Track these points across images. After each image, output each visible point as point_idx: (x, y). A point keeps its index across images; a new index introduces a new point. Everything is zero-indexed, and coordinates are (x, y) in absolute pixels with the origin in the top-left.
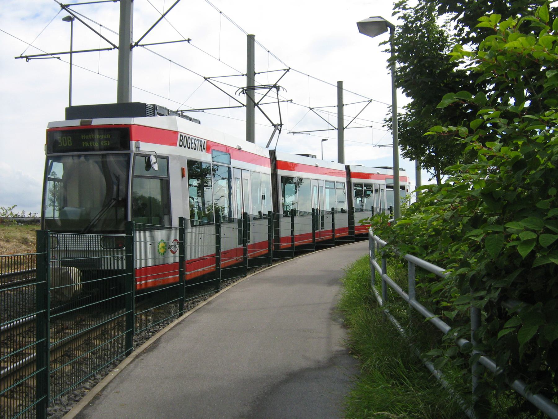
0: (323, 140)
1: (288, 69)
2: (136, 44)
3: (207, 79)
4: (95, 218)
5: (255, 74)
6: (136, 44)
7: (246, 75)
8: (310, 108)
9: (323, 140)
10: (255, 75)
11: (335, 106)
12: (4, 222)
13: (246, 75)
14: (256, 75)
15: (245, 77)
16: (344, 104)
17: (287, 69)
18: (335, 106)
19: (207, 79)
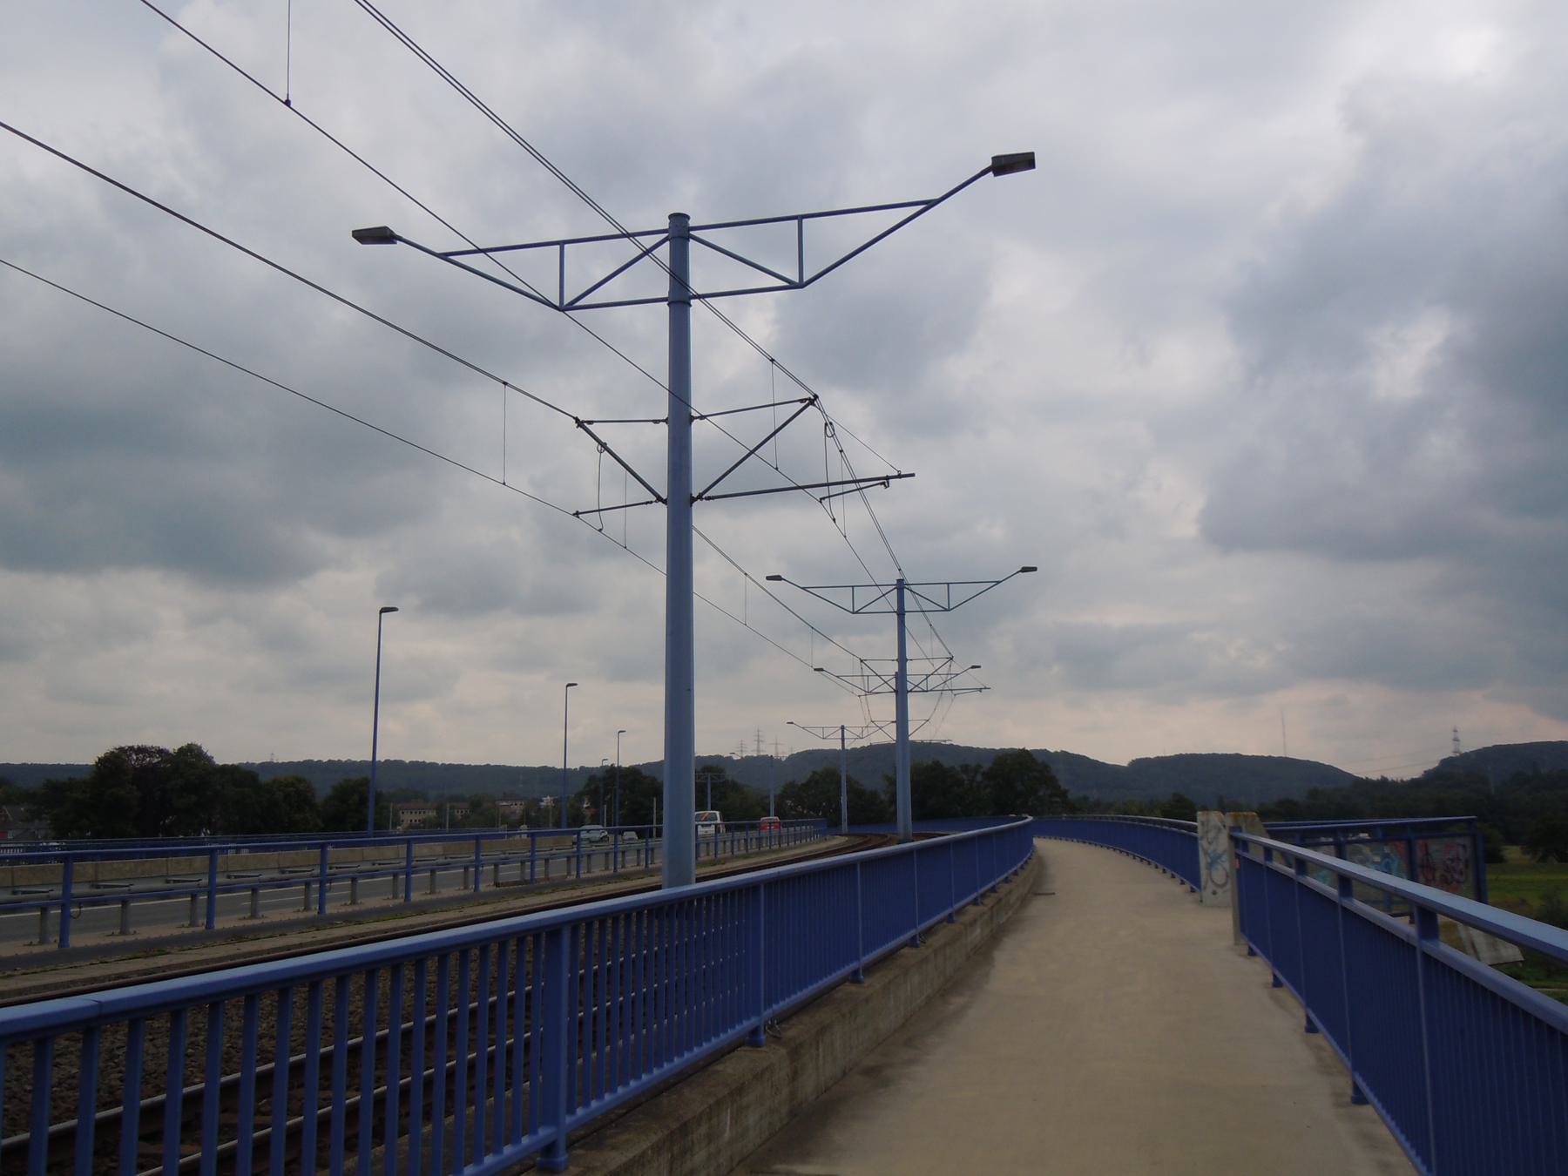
0: (384, 610)
1: (812, 398)
2: (700, 497)
3: (585, 424)
4: (174, 876)
5: (692, 419)
6: (700, 497)
7: (665, 421)
8: (577, 420)
9: (384, 610)
10: (693, 424)
11: (656, 422)
12: (296, 1051)
13: (665, 421)
14: (695, 423)
15: (664, 427)
16: (908, 658)
17: (810, 399)
18: (656, 422)
19: (585, 424)
